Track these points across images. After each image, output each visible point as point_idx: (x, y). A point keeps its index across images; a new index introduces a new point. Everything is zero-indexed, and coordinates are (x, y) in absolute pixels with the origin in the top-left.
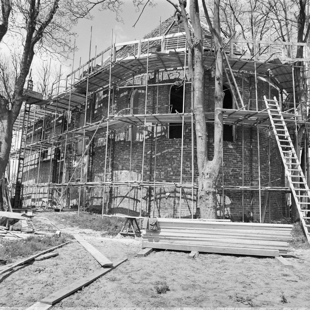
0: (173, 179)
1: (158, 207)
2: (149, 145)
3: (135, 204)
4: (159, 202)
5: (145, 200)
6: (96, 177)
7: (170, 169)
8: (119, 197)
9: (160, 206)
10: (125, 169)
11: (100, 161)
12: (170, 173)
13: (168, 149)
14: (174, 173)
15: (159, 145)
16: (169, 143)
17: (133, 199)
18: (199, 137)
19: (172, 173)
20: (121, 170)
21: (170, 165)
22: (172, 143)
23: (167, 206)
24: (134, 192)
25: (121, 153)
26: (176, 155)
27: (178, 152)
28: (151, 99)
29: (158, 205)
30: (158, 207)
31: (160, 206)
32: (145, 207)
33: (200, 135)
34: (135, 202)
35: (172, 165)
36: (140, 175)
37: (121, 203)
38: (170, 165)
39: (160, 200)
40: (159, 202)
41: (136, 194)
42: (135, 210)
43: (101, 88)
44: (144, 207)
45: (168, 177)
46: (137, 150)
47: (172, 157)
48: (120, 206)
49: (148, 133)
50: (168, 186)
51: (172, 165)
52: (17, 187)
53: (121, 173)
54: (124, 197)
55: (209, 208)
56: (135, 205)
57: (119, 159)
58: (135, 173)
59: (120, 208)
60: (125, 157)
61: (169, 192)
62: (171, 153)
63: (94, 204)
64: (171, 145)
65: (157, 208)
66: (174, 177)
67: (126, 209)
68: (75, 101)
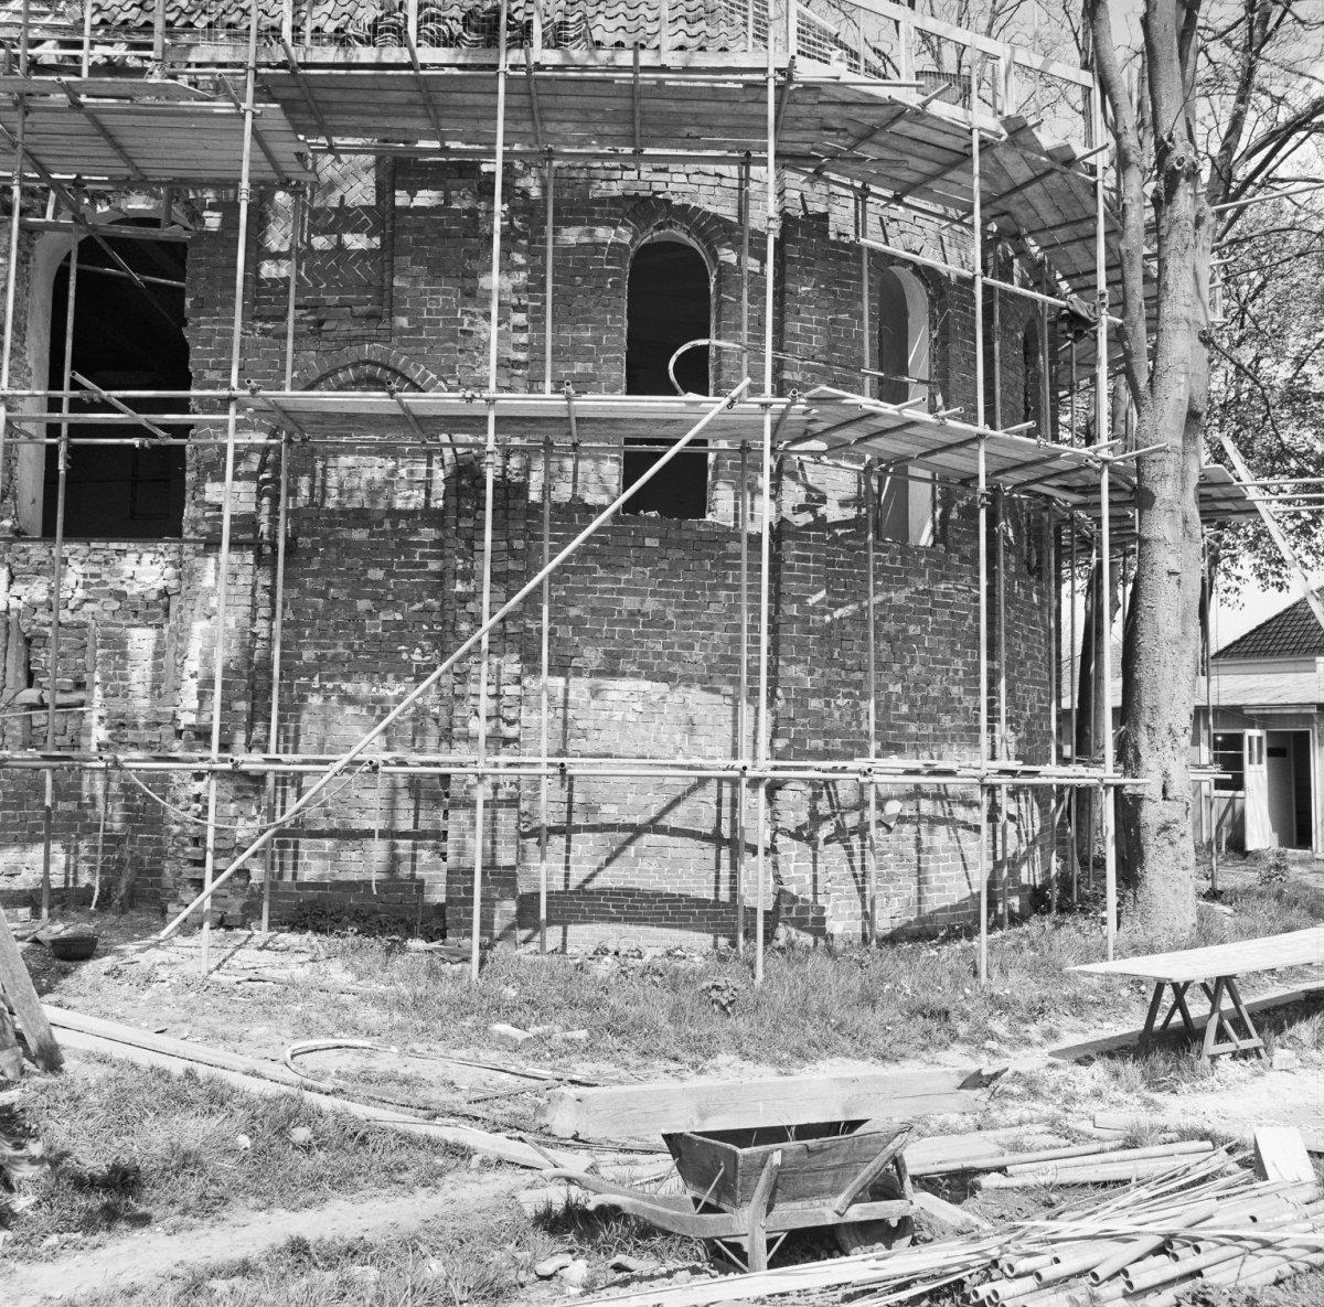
0: (910, 737)
1: (859, 871)
2: (816, 560)
3: (725, 863)
4: (857, 850)
5: (803, 845)
6: (315, 700)
7: (898, 688)
8: (593, 829)
9: (863, 867)
10: (635, 675)
11: (363, 605)
12: (897, 708)
13: (888, 590)
14: (912, 706)
15: (850, 565)
16: (893, 560)
17: (706, 838)
18: (1170, 573)
19: (904, 709)
20: (598, 673)
21: (896, 667)
22: (904, 562)
23: (892, 867)
24: (713, 800)
25: (595, 580)
26: (920, 622)
27: (925, 612)
28: (819, 322)
29: (857, 864)
30: (859, 871)
31: (863, 867)
32: (809, 880)
33: (1174, 567)
34: (725, 852)
35: (904, 668)
36: (746, 711)
37: (609, 861)
38: (896, 667)
39: (863, 838)
40: (857, 850)
41: (726, 811)
42: (725, 896)
43: (436, 145)
44: (802, 880)
45: (891, 727)
46: (725, 576)
47: (905, 630)
48: (603, 881)
49: (808, 498)
50: (889, 771)
51: (904, 668)
52: (437, 832)
53: (595, 693)
54: (637, 831)
55: (1185, 869)
56: (725, 872)
57: (573, 612)
58: (718, 699)
59: (601, 892)
60: (630, 603)
61: (898, 798)
62: (899, 609)
63: (306, 876)
64: (898, 571)
65: (851, 879)
66: (912, 728)
67: (657, 894)
68: (130, 152)
